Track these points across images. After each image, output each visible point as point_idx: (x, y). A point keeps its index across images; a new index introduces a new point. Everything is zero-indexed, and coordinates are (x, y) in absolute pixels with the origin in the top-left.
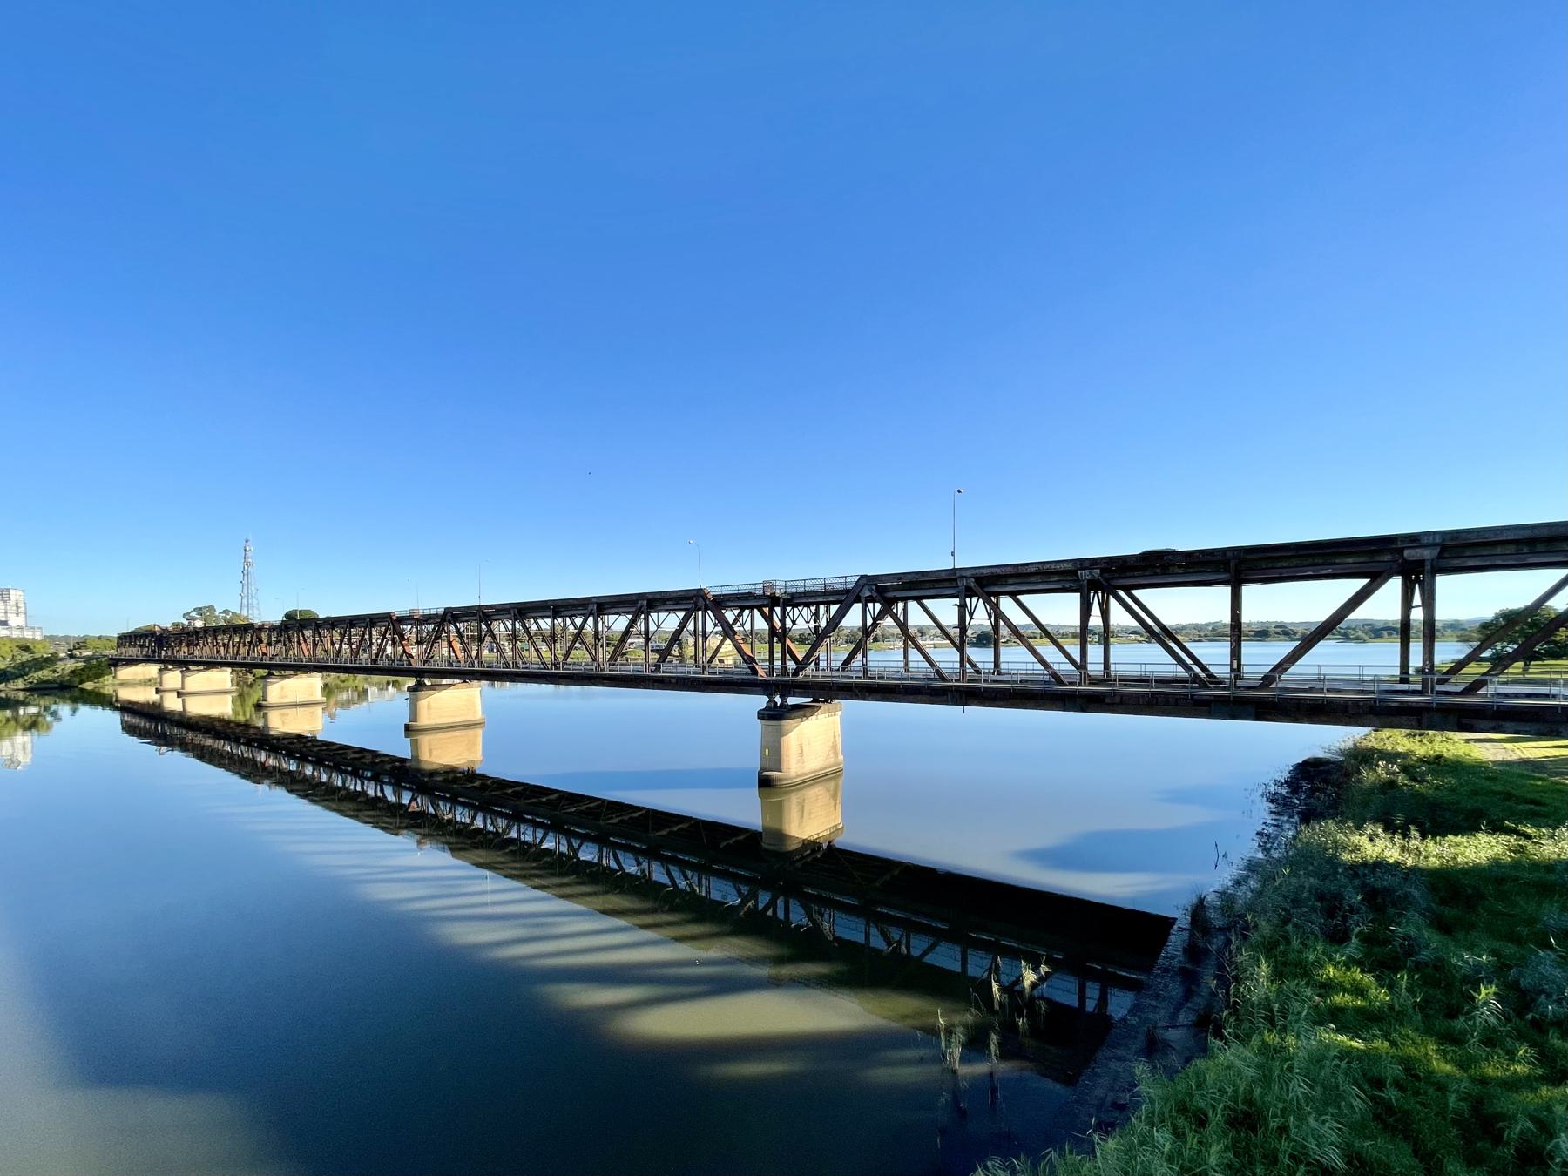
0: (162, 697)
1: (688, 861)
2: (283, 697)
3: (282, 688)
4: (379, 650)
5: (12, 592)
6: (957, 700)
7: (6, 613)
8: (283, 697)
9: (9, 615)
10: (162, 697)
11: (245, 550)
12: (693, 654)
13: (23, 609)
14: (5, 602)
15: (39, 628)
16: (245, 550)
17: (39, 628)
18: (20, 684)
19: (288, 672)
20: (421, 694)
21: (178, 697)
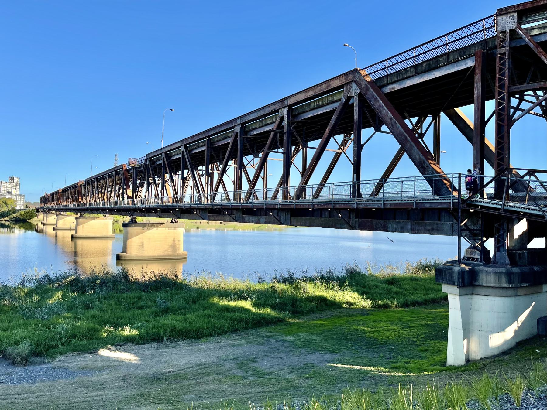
0: (56, 232)
1: (357, 193)
2: (64, 225)
3: (64, 221)
4: (405, 337)
5: (15, 179)
6: (241, 309)
7: (11, 188)
8: (64, 225)
9: (12, 189)
10: (56, 232)
11: (115, 160)
12: (485, 284)
13: (18, 186)
14: (11, 183)
15: (24, 195)
16: (115, 160)
17: (24, 195)
18: (7, 218)
19: (68, 213)
20: (132, 230)
21: (54, 230)
